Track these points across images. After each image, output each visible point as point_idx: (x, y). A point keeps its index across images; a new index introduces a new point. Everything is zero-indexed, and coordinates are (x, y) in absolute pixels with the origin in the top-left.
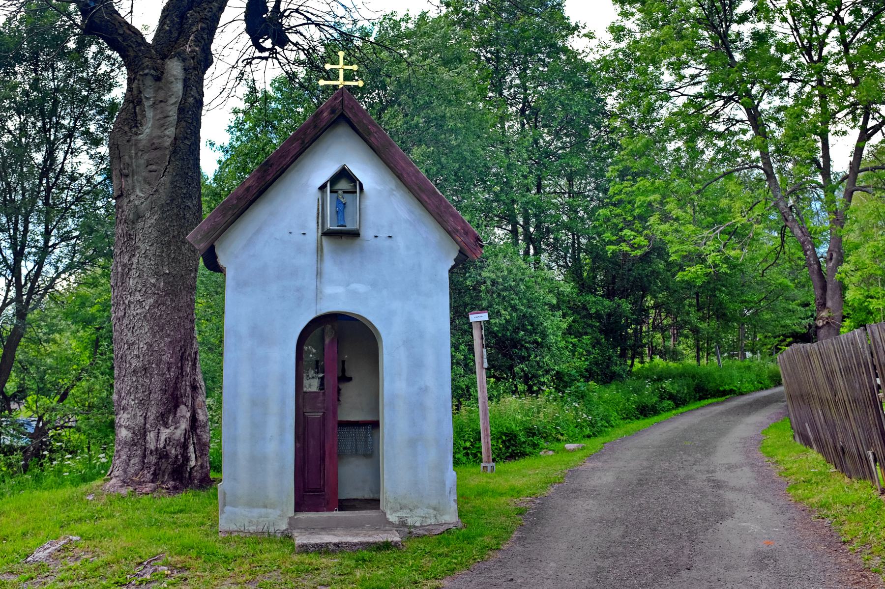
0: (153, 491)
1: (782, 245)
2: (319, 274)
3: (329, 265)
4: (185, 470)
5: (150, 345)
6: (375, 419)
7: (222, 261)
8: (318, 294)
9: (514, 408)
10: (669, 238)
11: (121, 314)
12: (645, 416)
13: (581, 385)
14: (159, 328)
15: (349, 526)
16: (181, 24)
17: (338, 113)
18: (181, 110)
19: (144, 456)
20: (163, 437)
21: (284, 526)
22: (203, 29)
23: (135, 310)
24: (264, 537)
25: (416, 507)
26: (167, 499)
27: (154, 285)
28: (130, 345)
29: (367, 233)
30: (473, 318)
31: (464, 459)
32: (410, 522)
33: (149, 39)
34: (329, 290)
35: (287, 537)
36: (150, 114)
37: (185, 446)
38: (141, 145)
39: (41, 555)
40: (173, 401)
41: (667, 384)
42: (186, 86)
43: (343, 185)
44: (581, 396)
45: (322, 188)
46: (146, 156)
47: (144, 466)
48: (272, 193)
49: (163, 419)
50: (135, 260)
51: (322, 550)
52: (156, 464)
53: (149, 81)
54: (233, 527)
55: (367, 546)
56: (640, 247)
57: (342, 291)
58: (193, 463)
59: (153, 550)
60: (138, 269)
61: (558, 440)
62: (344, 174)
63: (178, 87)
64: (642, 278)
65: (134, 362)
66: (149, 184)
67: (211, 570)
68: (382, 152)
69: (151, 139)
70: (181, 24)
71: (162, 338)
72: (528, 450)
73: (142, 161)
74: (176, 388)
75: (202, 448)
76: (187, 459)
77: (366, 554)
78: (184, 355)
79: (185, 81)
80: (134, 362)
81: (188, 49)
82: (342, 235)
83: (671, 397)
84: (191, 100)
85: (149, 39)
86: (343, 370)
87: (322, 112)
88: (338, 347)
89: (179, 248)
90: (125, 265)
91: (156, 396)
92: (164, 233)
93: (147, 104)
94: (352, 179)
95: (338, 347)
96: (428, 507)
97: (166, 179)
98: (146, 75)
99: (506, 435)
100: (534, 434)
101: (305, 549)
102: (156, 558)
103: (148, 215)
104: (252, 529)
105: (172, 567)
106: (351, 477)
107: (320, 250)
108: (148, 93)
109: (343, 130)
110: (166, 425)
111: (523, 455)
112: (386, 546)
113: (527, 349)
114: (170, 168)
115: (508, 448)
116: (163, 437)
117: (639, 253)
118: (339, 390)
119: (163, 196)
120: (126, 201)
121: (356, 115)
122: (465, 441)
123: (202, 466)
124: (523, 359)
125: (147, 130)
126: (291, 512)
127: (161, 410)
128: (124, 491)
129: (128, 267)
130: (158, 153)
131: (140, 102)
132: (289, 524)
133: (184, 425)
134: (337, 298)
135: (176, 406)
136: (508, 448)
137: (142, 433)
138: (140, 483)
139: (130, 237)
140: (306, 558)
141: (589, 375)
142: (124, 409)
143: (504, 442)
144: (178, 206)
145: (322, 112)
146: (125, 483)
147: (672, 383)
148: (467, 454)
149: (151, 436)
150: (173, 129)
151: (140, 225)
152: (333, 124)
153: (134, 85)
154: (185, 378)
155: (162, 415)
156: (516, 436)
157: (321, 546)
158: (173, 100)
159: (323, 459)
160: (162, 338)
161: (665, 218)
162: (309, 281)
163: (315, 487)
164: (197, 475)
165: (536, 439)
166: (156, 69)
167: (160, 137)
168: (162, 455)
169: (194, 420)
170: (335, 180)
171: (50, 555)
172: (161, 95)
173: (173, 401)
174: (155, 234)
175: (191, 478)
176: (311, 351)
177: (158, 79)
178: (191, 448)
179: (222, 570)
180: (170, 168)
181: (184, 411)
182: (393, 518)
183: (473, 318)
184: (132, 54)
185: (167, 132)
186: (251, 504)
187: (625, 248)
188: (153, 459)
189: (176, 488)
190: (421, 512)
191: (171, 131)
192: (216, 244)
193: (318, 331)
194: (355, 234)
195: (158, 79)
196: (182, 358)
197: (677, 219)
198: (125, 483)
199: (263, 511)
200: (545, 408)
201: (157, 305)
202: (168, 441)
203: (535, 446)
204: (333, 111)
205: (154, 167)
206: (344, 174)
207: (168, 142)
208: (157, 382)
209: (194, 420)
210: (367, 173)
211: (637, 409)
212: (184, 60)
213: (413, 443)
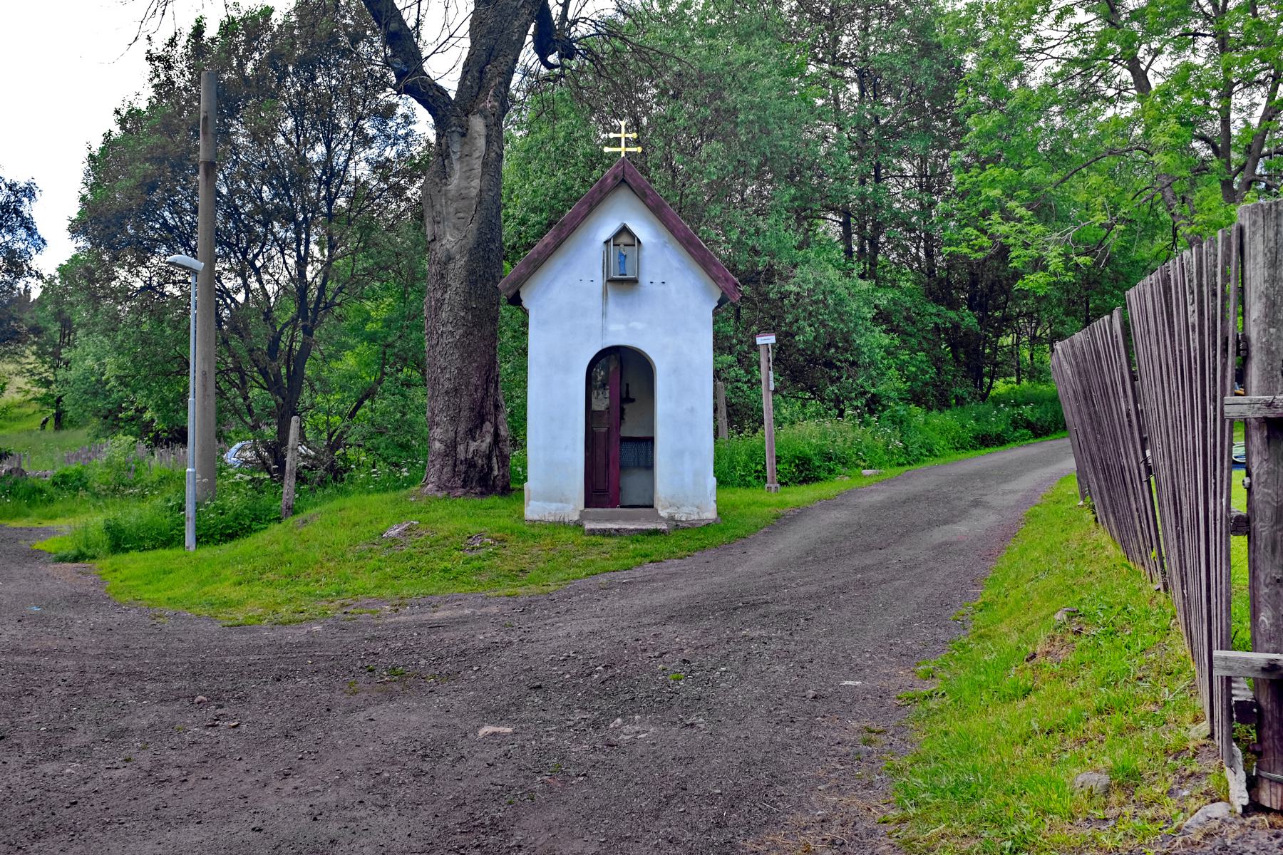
0: (465, 494)
1: (1174, 243)
2: (604, 314)
3: (611, 305)
4: (491, 474)
5: (460, 370)
6: (649, 435)
7: (525, 304)
8: (604, 329)
9: (811, 432)
10: (1011, 241)
11: (434, 342)
12: (987, 446)
13: (901, 409)
14: (467, 355)
15: (628, 519)
16: (481, 79)
17: (620, 179)
18: (485, 164)
19: (455, 465)
20: (471, 450)
21: (576, 518)
22: (500, 83)
23: (447, 340)
24: (561, 524)
25: (683, 505)
26: (478, 500)
28: (443, 369)
29: (645, 279)
30: (760, 340)
31: (755, 482)
32: (677, 517)
33: (452, 95)
34: (613, 327)
35: (578, 525)
36: (457, 166)
37: (489, 458)
38: (450, 195)
39: (393, 533)
40: (480, 417)
41: (1026, 411)
42: (488, 142)
43: (625, 239)
44: (899, 422)
45: (607, 242)
46: (455, 205)
47: (455, 473)
48: (565, 246)
49: (471, 433)
50: (447, 296)
51: (605, 533)
52: (466, 472)
53: (456, 137)
54: (536, 517)
55: (641, 531)
56: (981, 249)
57: (623, 330)
58: (496, 473)
59: (478, 529)
60: (449, 304)
61: (857, 466)
62: (624, 230)
63: (481, 143)
64: (1000, 282)
65: (447, 385)
67: (523, 542)
68: (657, 209)
69: (459, 189)
70: (481, 79)
71: (470, 363)
72: (823, 475)
73: (451, 210)
74: (482, 407)
75: (504, 460)
76: (491, 469)
77: (640, 537)
78: (490, 377)
79: (488, 136)
80: (447, 385)
81: (489, 105)
82: (622, 282)
83: (1029, 425)
84: (493, 154)
85: (452, 95)
86: (628, 392)
87: (606, 178)
88: (621, 379)
89: (485, 285)
90: (438, 300)
92: (471, 272)
93: (454, 157)
94: (632, 235)
95: (621, 379)
96: (693, 505)
97: (473, 227)
99: (798, 458)
100: (830, 459)
101: (592, 532)
102: (480, 535)
103: (458, 257)
104: (551, 519)
105: (495, 540)
106: (632, 484)
107: (605, 293)
108: (456, 147)
109: (624, 185)
110: (474, 439)
111: (817, 479)
112: (656, 532)
113: (839, 369)
114: (477, 217)
115: (801, 472)
116: (471, 450)
117: (980, 255)
118: (622, 411)
119: (471, 240)
120: (438, 244)
121: (634, 180)
122: (757, 464)
123: (503, 476)
124: (833, 381)
125: (455, 181)
126: (582, 507)
127: (1262, 326)
128: (439, 494)
129: (440, 302)
130: (466, 203)
131: (448, 156)
133: (488, 439)
134: (619, 335)
135: (482, 423)
136: (801, 472)
137: (452, 446)
138: (452, 488)
139: (442, 277)
140: (594, 539)
141: (916, 398)
142: (438, 424)
143: (797, 466)
144: (484, 250)
145: (606, 178)
146: (440, 488)
147: (1032, 410)
148: (758, 477)
149: (461, 448)
150: (478, 181)
151: (451, 266)
152: (616, 187)
153: (443, 141)
154: (491, 401)
155: (471, 430)
156: (810, 460)
157: (605, 530)
158: (477, 154)
159: (607, 466)
160: (470, 363)
161: (1007, 216)
162: (596, 320)
163: (600, 489)
164: (499, 483)
165: (832, 465)
166: (461, 127)
168: (470, 464)
169: (496, 435)
170: (617, 235)
171: (399, 533)
172: (467, 149)
173: (480, 417)
174: (464, 273)
175: (494, 486)
176: (600, 374)
177: (464, 135)
178: (494, 459)
179: (531, 542)
180: (477, 217)
181: (488, 427)
182: (663, 513)
183: (760, 340)
184: (440, 113)
185: (473, 184)
186: (549, 499)
187: (964, 249)
188: (463, 468)
189: (482, 494)
190: (685, 509)
191: (476, 183)
192: (521, 290)
193: (603, 361)
194: (635, 281)
195: (464, 135)
196: (487, 381)
197: (1020, 220)
198: (440, 488)
199: (560, 505)
200: (842, 432)
201: (465, 335)
202: (476, 452)
203: (831, 471)
204: (615, 178)
205: (462, 215)
206: (624, 230)
207: (474, 192)
208: (465, 402)
209: (496, 435)
210: (643, 229)
211: (976, 438)
212: (486, 117)
213: (679, 454)
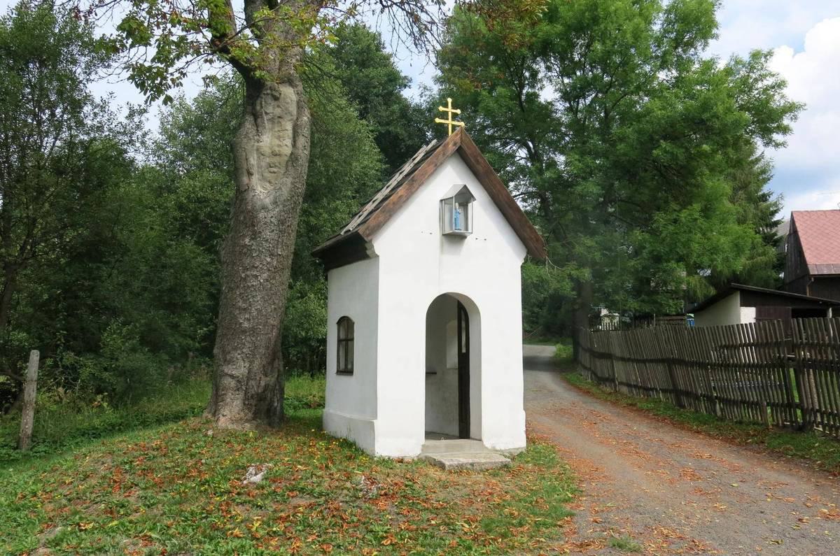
20: (263, 383)
27: (268, 263)
66: (270, 182)
91: (262, 351)
97: (289, 181)
98: (268, 94)
132: (422, 450)
167: (279, 146)
202: (266, 386)
